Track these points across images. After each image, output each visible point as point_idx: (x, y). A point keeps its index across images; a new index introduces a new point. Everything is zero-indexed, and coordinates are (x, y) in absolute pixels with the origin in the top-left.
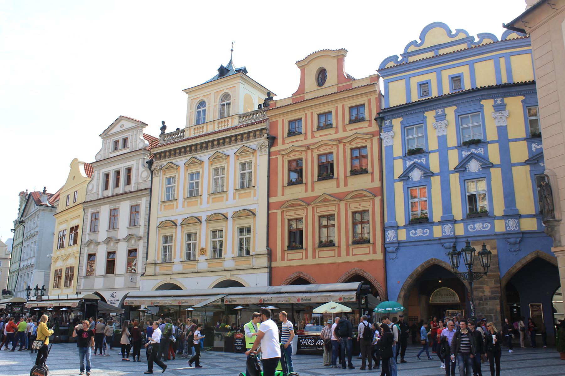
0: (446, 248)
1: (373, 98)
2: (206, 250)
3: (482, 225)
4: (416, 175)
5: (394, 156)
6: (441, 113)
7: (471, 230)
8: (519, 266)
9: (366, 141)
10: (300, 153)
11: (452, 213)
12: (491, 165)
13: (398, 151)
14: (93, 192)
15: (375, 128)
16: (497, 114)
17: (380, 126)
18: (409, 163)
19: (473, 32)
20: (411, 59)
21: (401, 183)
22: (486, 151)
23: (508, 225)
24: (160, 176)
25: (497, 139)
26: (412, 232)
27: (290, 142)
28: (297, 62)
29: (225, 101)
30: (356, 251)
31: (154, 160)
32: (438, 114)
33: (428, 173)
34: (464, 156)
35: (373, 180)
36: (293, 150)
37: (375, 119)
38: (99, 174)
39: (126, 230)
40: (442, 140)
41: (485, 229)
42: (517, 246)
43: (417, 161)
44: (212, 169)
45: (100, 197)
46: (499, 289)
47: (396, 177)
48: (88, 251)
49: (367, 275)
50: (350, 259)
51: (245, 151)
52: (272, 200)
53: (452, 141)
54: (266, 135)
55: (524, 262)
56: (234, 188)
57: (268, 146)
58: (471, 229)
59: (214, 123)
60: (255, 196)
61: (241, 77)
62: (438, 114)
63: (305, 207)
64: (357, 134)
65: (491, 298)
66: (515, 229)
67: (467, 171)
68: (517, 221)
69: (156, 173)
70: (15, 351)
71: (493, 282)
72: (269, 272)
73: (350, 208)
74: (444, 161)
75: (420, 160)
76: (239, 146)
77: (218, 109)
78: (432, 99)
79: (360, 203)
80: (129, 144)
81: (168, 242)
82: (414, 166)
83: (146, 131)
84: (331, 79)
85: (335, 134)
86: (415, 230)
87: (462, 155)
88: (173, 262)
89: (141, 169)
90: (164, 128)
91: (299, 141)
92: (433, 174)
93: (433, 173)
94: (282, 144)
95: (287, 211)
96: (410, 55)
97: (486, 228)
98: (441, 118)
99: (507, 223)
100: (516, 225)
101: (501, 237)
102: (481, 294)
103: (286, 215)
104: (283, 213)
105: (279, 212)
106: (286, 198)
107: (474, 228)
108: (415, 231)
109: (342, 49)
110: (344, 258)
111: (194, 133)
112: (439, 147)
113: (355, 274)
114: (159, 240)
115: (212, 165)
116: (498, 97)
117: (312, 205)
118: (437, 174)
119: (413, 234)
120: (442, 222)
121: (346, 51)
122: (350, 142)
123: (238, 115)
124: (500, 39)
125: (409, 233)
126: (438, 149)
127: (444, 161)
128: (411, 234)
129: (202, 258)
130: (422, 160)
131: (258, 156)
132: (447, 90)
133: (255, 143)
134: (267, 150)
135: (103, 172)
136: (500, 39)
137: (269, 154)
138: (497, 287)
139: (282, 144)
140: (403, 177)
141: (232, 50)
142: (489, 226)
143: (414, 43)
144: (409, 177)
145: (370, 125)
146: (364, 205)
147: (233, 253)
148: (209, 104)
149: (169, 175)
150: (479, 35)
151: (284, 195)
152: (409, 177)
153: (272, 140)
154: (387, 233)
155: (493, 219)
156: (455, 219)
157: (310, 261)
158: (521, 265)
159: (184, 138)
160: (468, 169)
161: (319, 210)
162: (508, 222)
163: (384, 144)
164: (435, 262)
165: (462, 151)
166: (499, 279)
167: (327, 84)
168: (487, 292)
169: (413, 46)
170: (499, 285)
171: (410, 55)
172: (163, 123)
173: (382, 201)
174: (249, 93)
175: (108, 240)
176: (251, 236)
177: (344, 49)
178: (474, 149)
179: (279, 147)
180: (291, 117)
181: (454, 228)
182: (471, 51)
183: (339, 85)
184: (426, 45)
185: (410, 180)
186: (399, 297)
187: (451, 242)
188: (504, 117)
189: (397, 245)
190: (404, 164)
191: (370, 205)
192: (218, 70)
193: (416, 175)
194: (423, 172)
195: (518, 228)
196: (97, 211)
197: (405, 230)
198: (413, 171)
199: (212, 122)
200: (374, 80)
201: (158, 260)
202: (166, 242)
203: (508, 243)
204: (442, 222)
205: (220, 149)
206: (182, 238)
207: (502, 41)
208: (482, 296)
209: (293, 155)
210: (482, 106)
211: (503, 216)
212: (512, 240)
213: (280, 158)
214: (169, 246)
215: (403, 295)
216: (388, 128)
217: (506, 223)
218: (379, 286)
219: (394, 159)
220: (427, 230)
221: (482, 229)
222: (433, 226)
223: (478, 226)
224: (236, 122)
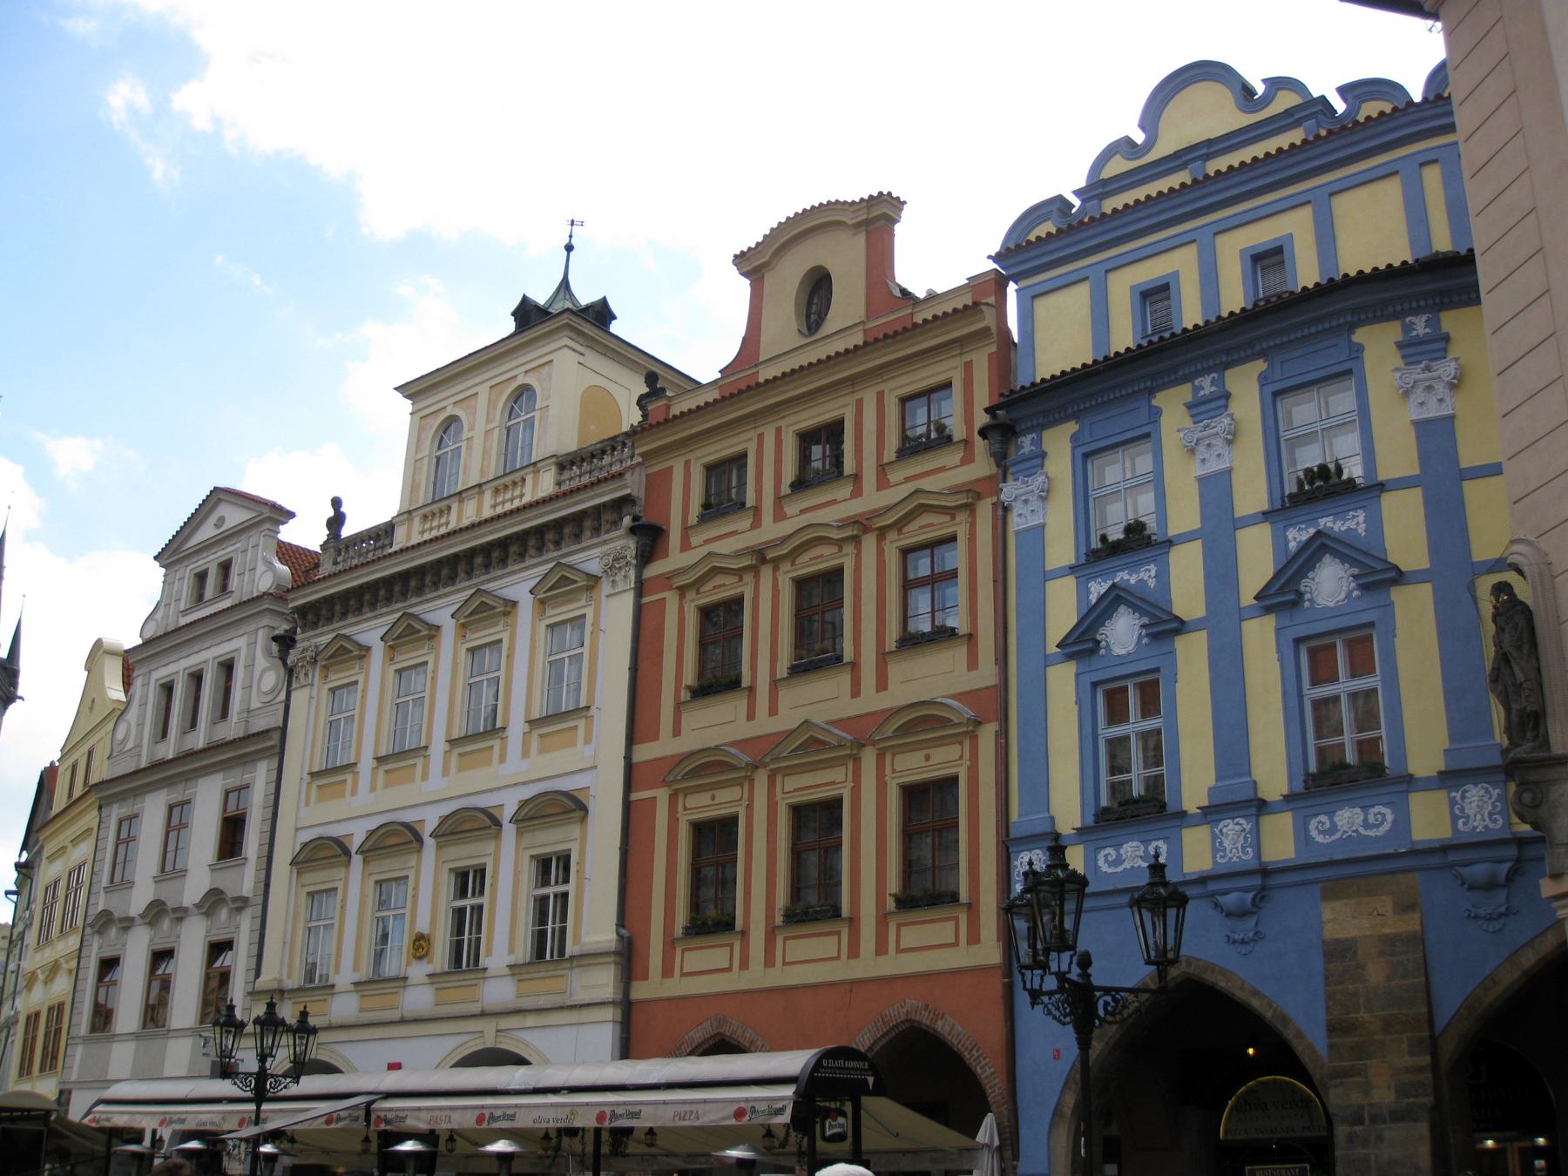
0: (1471, 888)
1: (981, 360)
2: (431, 941)
3: (1362, 817)
4: (1123, 633)
5: (1048, 567)
6: (1213, 389)
7: (1320, 839)
8: (1510, 978)
9: (953, 518)
10: (736, 579)
11: (1249, 774)
12: (1392, 574)
13: (1061, 550)
14: (126, 749)
15: (982, 466)
16: (1417, 373)
17: (1001, 458)
18: (1297, 536)
19: (1324, 84)
20: (1109, 205)
21: (1269, 623)
22: (1375, 523)
23: (1462, 809)
24: (312, 685)
25: (1416, 471)
26: (1106, 856)
27: (908, 480)
28: (735, 256)
29: (520, 416)
30: (911, 937)
31: (299, 630)
32: (1202, 393)
33: (1375, 572)
34: (1293, 546)
35: (973, 664)
36: (922, 505)
37: (983, 433)
38: (146, 685)
39: (152, 885)
40: (1216, 489)
41: (1372, 833)
42: (1501, 895)
43: (1126, 577)
44: (464, 650)
45: (143, 764)
46: (1427, 1077)
47: (1247, 597)
48: (100, 948)
49: (947, 1029)
50: (890, 965)
51: (564, 580)
52: (643, 753)
53: (1252, 494)
54: (627, 521)
55: (1529, 959)
56: (446, 737)
57: (636, 558)
58: (1320, 832)
59: (481, 493)
60: (588, 741)
61: (573, 329)
62: (1202, 393)
63: (743, 774)
64: (920, 495)
65: (1399, 1116)
66: (1491, 826)
67: (1307, 604)
68: (1495, 792)
69: (302, 676)
71: (1405, 1046)
72: (619, 1018)
73: (894, 771)
74: (1222, 571)
75: (1138, 572)
76: (540, 568)
77: (495, 445)
78: (1025, 392)
79: (930, 751)
80: (234, 583)
81: (469, 895)
82: (1320, 546)
83: (288, 533)
84: (847, 306)
85: (853, 501)
86: (1118, 846)
87: (1287, 542)
88: (485, 969)
89: (261, 662)
90: (336, 522)
91: (735, 533)
92: (1398, 577)
93: (1182, 622)
94: (879, 489)
95: (687, 792)
96: (1212, 149)
97: (1377, 826)
98: (1208, 408)
99: (1456, 803)
100: (1494, 807)
101: (1436, 860)
102: (1356, 1098)
103: (685, 809)
104: (673, 798)
105: (662, 795)
106: (689, 742)
107: (1333, 829)
108: (1118, 852)
109: (881, 193)
110: (869, 965)
111: (494, 506)
112: (1204, 517)
113: (908, 1025)
114: (296, 907)
115: (392, 659)
116: (1415, 312)
117: (675, 781)
118: (1198, 625)
119: (1111, 864)
120: (1213, 812)
121: (897, 204)
122: (899, 525)
123: (554, 459)
124: (1417, 97)
125: (1096, 859)
126: (1199, 526)
127: (1222, 571)
128: (1101, 862)
129: (418, 971)
130: (1143, 575)
131: (603, 598)
132: (1234, 298)
133: (596, 552)
134: (632, 574)
135: (157, 680)
136: (1417, 97)
137: (640, 589)
138: (1421, 1070)
139: (879, 489)
140: (1074, 643)
142: (1390, 817)
143: (1124, 146)
144: (1099, 642)
145: (968, 459)
146: (940, 761)
147: (511, 951)
148: (472, 428)
149: (337, 679)
150: (1344, 91)
151: (885, 688)
152: (1099, 642)
153: (650, 538)
154: (1018, 863)
155: (1404, 787)
156: (1260, 795)
157: (757, 976)
158: (1517, 974)
159: (391, 550)
160: (1307, 596)
161: (792, 783)
162: (1463, 797)
163: (1016, 523)
164: (1191, 971)
165: (1286, 528)
166: (1426, 1034)
167: (832, 323)
168: (1383, 1095)
169: (1118, 158)
170: (1426, 1060)
171: (1212, 149)
172: (336, 503)
173: (1003, 734)
174: (599, 381)
175: (156, 911)
176: (571, 888)
177: (890, 194)
178: (1331, 518)
179: (674, 559)
180: (716, 452)
181: (1257, 832)
182: (1357, 137)
183: (871, 325)
184: (1163, 149)
185: (1103, 652)
186: (1057, 1112)
187: (1246, 890)
188: (1440, 388)
189: (1256, 881)
190: (1083, 592)
191: (961, 758)
192: (513, 314)
193: (1123, 633)
194: (1146, 620)
195: (1501, 821)
196: (135, 812)
197: (1289, 814)
198: (1110, 617)
199: (476, 490)
200: (986, 290)
201: (289, 977)
202: (545, 882)
203: (1463, 883)
204: (1213, 812)
205: (489, 581)
206: (363, 895)
207: (1425, 100)
208: (1361, 1107)
210: (1360, 349)
211: (1440, 773)
212: (1479, 871)
213: (671, 599)
214: (556, 896)
215: (1072, 1106)
216: (1208, 407)
217: (1453, 802)
218: (988, 1072)
219: (1047, 576)
220: (1160, 843)
221: (1362, 830)
222: (1181, 827)
223: (1348, 818)
224: (546, 483)
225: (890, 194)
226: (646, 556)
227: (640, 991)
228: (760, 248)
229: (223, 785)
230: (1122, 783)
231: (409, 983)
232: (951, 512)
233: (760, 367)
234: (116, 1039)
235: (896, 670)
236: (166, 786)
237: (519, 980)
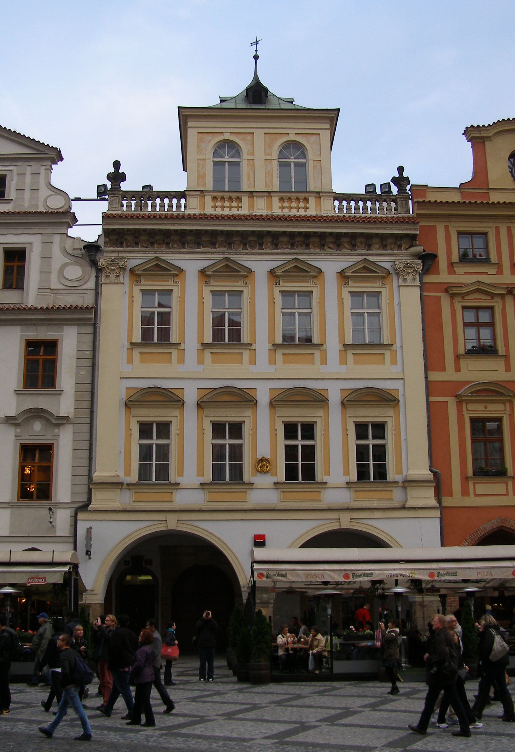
10: (489, 298)
60: (394, 362)
70: (112, 716)
91: (486, 273)
95: (468, 402)
129: (267, 480)
141: (256, 57)
172: (117, 164)
177: (472, 126)
209: (475, 299)
225: (472, 126)
226: (426, 271)
227: (447, 502)
228: (489, 128)
229: (22, 336)
230: (163, 445)
231: (254, 486)
232: (492, 295)
233: (490, 191)
234: (59, 506)
235: (463, 363)
236: (79, 325)
237: (355, 491)
